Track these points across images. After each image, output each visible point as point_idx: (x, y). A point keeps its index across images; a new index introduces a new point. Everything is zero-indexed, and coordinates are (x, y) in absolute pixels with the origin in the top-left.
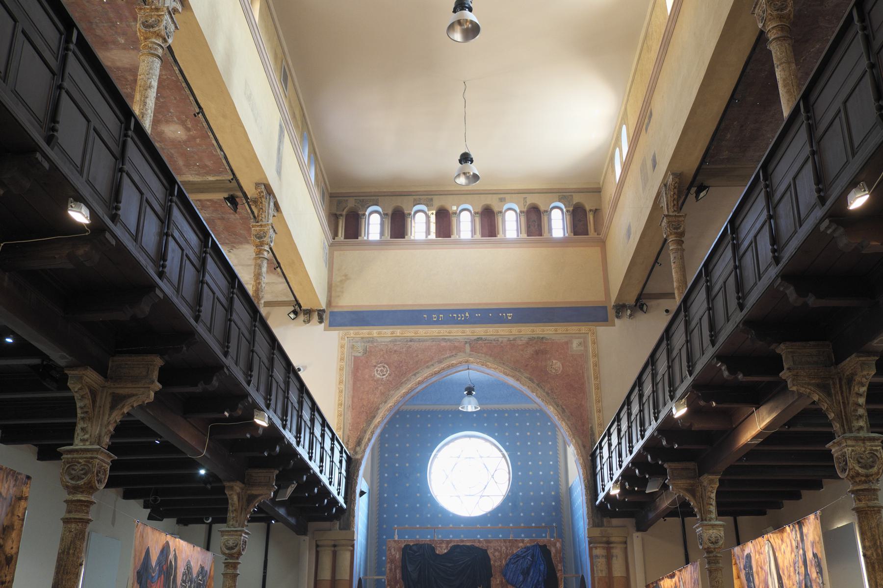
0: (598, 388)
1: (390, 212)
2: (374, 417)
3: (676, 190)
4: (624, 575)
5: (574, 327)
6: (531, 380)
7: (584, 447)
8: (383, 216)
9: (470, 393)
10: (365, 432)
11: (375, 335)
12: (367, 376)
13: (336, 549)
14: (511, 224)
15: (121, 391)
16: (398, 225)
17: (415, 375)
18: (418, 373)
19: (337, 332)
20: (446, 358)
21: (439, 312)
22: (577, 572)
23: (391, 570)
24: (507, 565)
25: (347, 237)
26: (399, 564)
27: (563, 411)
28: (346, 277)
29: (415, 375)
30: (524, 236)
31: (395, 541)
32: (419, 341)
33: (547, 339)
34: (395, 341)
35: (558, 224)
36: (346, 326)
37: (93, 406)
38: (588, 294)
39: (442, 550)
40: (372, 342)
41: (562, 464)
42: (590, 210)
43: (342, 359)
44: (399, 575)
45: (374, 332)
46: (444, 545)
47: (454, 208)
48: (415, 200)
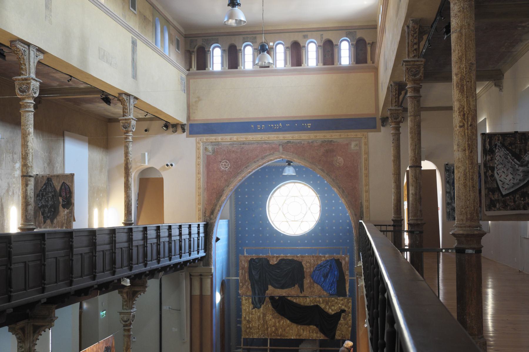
0: (367, 176)
1: (227, 48)
2: (221, 196)
3: (397, 92)
5: (352, 133)
6: (322, 170)
7: (356, 215)
8: (223, 51)
9: (289, 164)
10: (216, 205)
12: (215, 169)
13: (202, 277)
14: (312, 54)
15: (37, 324)
16: (233, 59)
18: (248, 166)
23: (242, 274)
24: (314, 271)
25: (198, 69)
26: (247, 270)
27: (343, 192)
28: (199, 99)
29: (246, 167)
30: (321, 65)
31: (244, 256)
32: (249, 144)
34: (233, 144)
35: (345, 54)
36: (200, 134)
37: (24, 336)
38: (364, 108)
39: (274, 262)
40: (218, 145)
42: (369, 44)
44: (247, 277)
45: (219, 138)
46: (275, 259)
47: (271, 44)
48: (244, 38)
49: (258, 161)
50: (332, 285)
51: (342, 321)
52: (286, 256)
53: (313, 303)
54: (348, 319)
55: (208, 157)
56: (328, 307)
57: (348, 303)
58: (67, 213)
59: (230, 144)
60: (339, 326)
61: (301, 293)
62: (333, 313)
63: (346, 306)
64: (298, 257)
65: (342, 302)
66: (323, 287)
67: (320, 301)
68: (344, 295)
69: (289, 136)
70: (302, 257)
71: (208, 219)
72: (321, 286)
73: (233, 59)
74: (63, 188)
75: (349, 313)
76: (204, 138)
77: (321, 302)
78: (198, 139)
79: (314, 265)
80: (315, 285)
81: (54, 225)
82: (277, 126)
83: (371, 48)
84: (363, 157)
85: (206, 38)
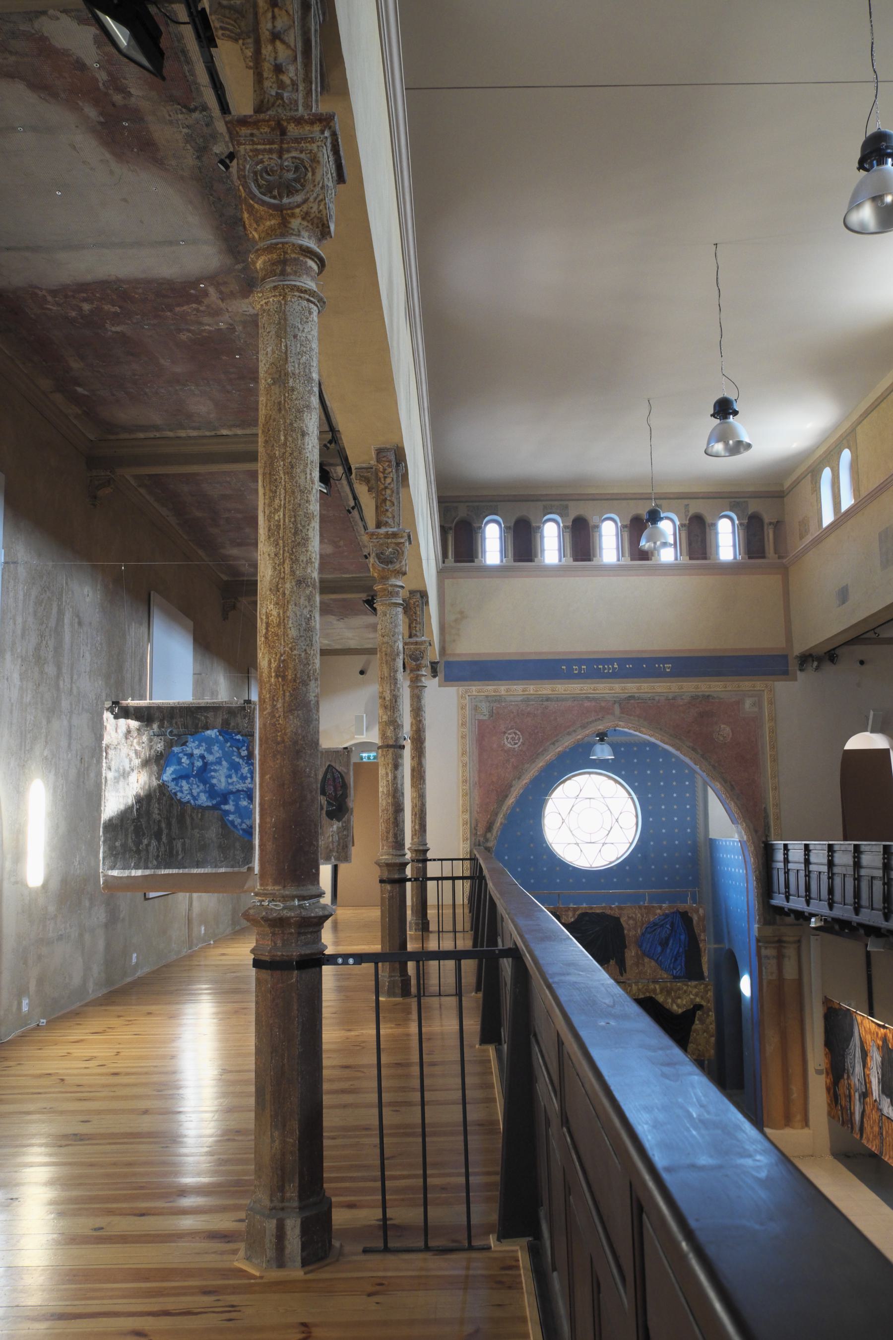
0: (774, 760)
2: (507, 796)
4: (797, 977)
6: (694, 749)
7: (756, 831)
9: (602, 740)
10: (497, 814)
11: (503, 693)
12: (495, 746)
16: (523, 543)
17: (553, 744)
19: (455, 688)
20: (591, 722)
21: (580, 662)
22: (718, 938)
24: (643, 934)
28: (462, 615)
32: (557, 700)
33: (713, 698)
34: (528, 700)
38: (763, 639)
40: (499, 701)
42: (770, 523)
43: (463, 724)
45: (502, 689)
46: (570, 914)
48: (545, 507)
49: (575, 731)
50: (676, 959)
51: (697, 1025)
52: (592, 908)
53: (644, 993)
54: (708, 1021)
56: (670, 1001)
57: (706, 992)
58: (338, 828)
59: (522, 701)
60: (693, 1035)
61: (622, 975)
62: (680, 1011)
63: (702, 998)
64: (613, 908)
65: (695, 991)
66: (660, 964)
67: (655, 990)
68: (700, 976)
69: (632, 687)
70: (620, 908)
71: (482, 839)
72: (656, 961)
73: (523, 543)
74: (329, 776)
76: (474, 688)
77: (658, 990)
79: (643, 924)
80: (646, 960)
82: (609, 669)
83: (774, 532)
84: (767, 726)
85: (477, 504)
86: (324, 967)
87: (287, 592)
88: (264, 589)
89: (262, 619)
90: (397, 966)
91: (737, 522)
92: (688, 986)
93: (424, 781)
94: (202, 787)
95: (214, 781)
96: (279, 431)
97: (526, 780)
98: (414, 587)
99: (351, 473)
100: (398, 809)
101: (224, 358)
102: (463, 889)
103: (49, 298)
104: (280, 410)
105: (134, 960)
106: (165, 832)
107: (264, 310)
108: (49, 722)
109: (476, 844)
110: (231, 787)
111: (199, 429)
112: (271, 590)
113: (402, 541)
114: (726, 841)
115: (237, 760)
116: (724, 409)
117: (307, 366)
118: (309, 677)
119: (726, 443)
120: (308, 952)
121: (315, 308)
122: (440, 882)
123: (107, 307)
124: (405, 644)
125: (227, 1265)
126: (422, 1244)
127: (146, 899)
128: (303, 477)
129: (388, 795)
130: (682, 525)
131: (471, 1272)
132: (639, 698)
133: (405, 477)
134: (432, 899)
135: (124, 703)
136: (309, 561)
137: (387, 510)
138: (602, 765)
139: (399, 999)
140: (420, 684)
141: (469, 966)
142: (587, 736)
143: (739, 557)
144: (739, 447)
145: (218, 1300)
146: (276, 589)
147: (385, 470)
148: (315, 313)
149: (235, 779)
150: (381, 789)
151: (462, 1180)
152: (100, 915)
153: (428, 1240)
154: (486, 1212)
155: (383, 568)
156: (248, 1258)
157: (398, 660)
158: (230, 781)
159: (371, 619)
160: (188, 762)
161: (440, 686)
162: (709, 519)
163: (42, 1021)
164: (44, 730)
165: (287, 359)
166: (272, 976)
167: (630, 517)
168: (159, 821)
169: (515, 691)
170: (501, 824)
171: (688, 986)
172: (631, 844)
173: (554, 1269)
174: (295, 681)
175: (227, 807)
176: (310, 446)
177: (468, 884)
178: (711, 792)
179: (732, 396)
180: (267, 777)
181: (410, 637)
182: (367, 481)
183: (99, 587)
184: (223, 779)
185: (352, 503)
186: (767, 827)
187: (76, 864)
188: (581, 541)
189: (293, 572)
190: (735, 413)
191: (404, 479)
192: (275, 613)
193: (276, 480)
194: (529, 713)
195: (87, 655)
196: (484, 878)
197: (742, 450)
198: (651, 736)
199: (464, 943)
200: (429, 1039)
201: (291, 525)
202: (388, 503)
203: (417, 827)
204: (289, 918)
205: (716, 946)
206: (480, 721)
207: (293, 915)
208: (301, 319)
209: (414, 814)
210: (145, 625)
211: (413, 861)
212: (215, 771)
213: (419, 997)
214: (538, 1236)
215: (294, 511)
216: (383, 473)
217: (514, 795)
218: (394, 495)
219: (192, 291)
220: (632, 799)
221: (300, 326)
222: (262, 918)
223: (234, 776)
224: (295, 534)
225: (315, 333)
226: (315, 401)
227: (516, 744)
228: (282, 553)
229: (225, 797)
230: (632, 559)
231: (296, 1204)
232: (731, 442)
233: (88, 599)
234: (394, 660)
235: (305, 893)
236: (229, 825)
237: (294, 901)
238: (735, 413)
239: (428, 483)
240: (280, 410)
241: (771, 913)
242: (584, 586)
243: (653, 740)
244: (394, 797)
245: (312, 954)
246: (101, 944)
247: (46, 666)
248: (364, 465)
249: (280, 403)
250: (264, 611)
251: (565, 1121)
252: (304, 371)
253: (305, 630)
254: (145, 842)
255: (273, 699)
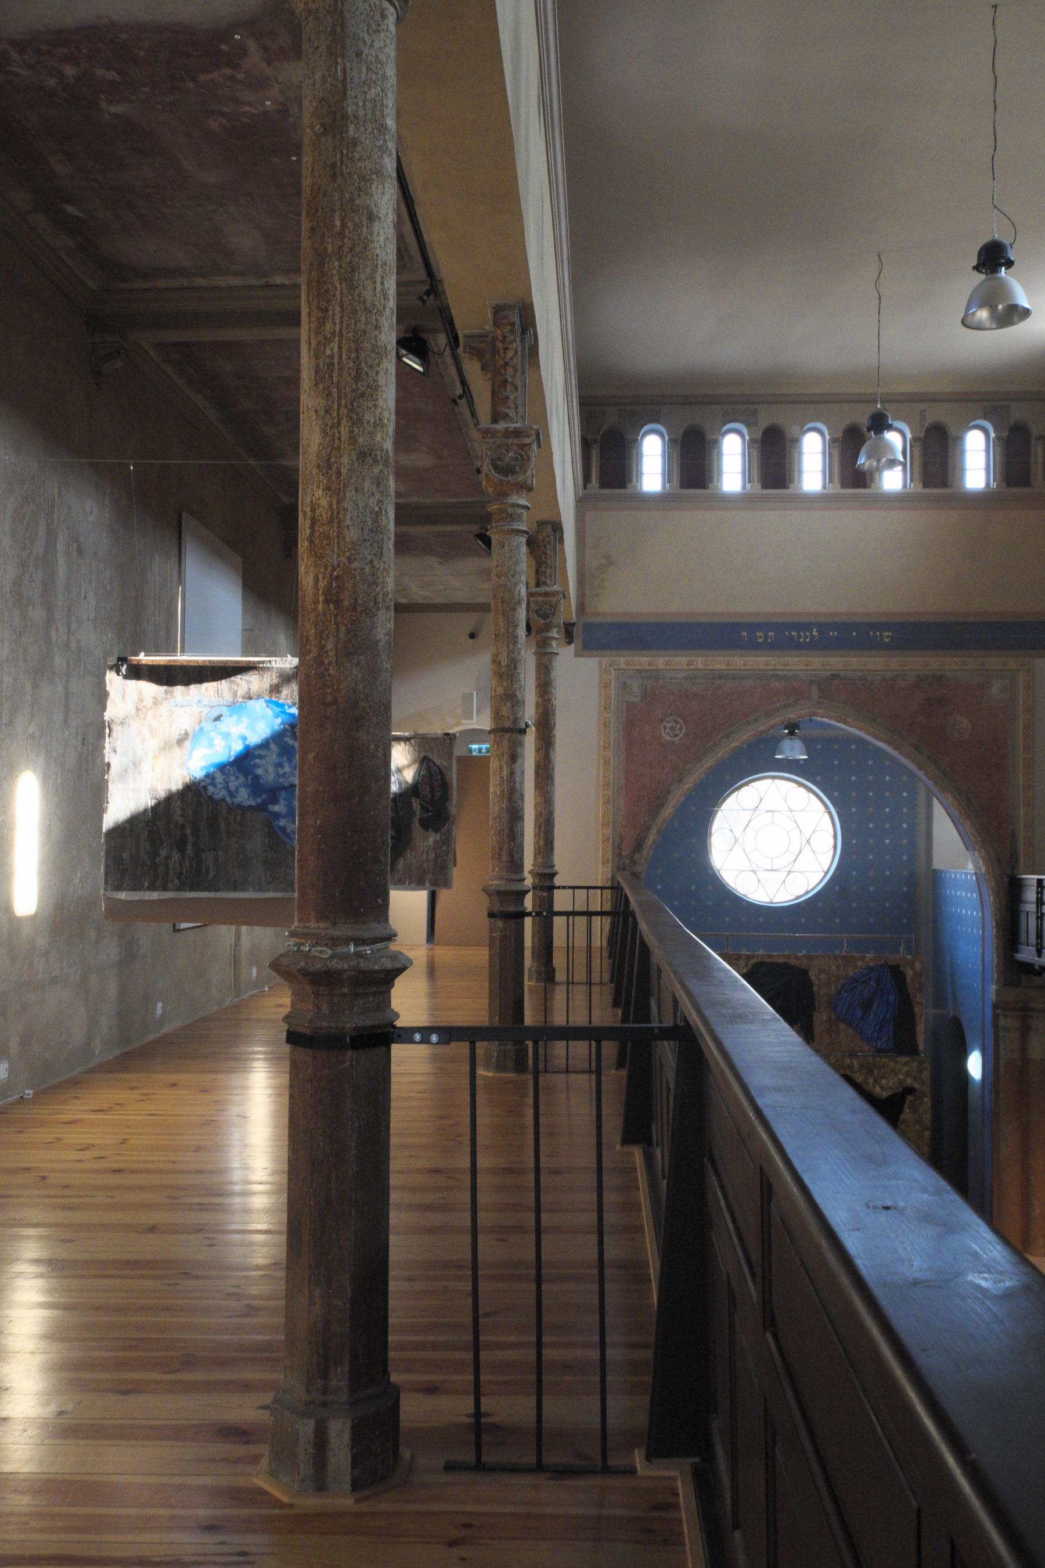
2: (662, 805)
7: (999, 861)
9: (792, 733)
10: (648, 829)
11: (661, 666)
16: (693, 464)
22: (939, 999)
24: (839, 992)
25: (604, 484)
28: (610, 561)
35: (976, 461)
41: (922, 828)
49: (756, 720)
52: (770, 956)
55: (630, 707)
56: (871, 1081)
58: (435, 842)
62: (884, 1095)
63: (915, 1079)
65: (906, 1069)
68: (912, 1050)
69: (835, 662)
70: (809, 958)
71: (627, 862)
75: (924, 1095)
76: (622, 660)
77: (856, 1066)
78: (605, 661)
80: (842, 1026)
81: (397, 876)
86: (394, 1047)
87: (344, 471)
88: (309, 466)
89: (305, 513)
90: (508, 1039)
91: (993, 435)
92: (896, 1062)
93: (552, 781)
94: (242, 779)
95: (259, 771)
96: (333, 210)
97: (688, 784)
98: (544, 516)
99: (458, 346)
100: (515, 816)
101: (275, 160)
102: (601, 927)
103: (14, 55)
104: (334, 177)
105: (159, 1010)
106: (191, 839)
107: (310, 11)
108: (35, 687)
109: (620, 868)
110: (281, 780)
111: (242, 274)
112: (318, 466)
113: (528, 441)
114: (955, 874)
115: (291, 742)
116: (993, 258)
117: (377, 105)
118: (376, 603)
119: (993, 308)
120: (368, 1023)
121: (392, 9)
122: (571, 918)
123: (99, 72)
124: (530, 595)
125: (242, 1482)
126: (531, 1459)
127: (176, 930)
128: (370, 287)
129: (502, 796)
130: (914, 439)
131: (605, 1512)
132: (845, 678)
133: (534, 350)
134: (559, 938)
135: (134, 659)
136: (379, 423)
137: (507, 397)
138: (791, 767)
139: (512, 1075)
140: (549, 650)
141: (610, 1049)
142: (772, 727)
143: (993, 485)
144: (1014, 314)
145: (223, 1543)
146: (326, 465)
147: (505, 337)
148: (391, 19)
149: (287, 769)
150: (492, 790)
151: (595, 1354)
152: (110, 951)
153: (542, 1455)
154: (628, 1409)
155: (500, 480)
156: (273, 1474)
157: (519, 610)
158: (281, 771)
159: (485, 563)
160: (223, 743)
161: (576, 655)
162: (952, 431)
163: (27, 1092)
164: (28, 698)
165: (345, 94)
166: (314, 1057)
167: (842, 428)
168: (183, 826)
169: (677, 664)
170: (654, 841)
171: (896, 1062)
172: (826, 873)
173: (736, 1526)
174: (354, 609)
175: (276, 808)
176: (382, 238)
177: (607, 921)
178: (937, 806)
179: (1006, 241)
180: (311, 756)
181: (538, 585)
182: (477, 353)
183: (107, 502)
184: (271, 769)
185: (459, 391)
186: (1014, 857)
187: (77, 881)
188: (774, 463)
189: (353, 440)
190: (1009, 264)
191: (533, 353)
192: (324, 503)
193: (327, 291)
194: (695, 695)
195: (91, 596)
196: (633, 914)
197: (1016, 319)
198: (860, 729)
199: (605, 1015)
200: (551, 1134)
201: (351, 364)
202: (509, 387)
203: (541, 843)
204: (339, 972)
205: (935, 1011)
206: (628, 704)
207: (346, 966)
208: (369, 26)
209: (538, 826)
210: (174, 559)
211: (534, 888)
212: (260, 757)
213: (536, 1074)
214: (706, 1452)
215: (356, 341)
216: (503, 342)
217: (672, 804)
218: (518, 374)
219: (224, 47)
220: (830, 813)
221: (366, 37)
222: (299, 971)
223: (286, 764)
224: (357, 378)
225: (391, 51)
226: (390, 165)
227: (677, 735)
228: (349, 434)
229: (273, 794)
230: (843, 487)
231: (343, 1397)
232: (1000, 307)
233: (91, 519)
234: (514, 609)
235: (367, 935)
236: (279, 832)
237: (348, 945)
238: (1009, 264)
239: (568, 394)
240: (334, 177)
241: (1014, 970)
242: (775, 522)
243: (863, 735)
244: (510, 800)
245: (374, 1026)
246: (112, 989)
247: (30, 607)
248: (475, 332)
249: (334, 165)
250: (308, 500)
251: (769, 1321)
252: (374, 114)
253: (371, 531)
254: (164, 853)
255: (320, 636)
